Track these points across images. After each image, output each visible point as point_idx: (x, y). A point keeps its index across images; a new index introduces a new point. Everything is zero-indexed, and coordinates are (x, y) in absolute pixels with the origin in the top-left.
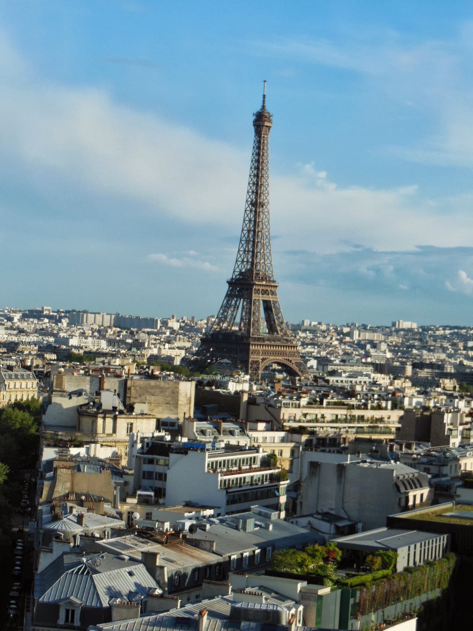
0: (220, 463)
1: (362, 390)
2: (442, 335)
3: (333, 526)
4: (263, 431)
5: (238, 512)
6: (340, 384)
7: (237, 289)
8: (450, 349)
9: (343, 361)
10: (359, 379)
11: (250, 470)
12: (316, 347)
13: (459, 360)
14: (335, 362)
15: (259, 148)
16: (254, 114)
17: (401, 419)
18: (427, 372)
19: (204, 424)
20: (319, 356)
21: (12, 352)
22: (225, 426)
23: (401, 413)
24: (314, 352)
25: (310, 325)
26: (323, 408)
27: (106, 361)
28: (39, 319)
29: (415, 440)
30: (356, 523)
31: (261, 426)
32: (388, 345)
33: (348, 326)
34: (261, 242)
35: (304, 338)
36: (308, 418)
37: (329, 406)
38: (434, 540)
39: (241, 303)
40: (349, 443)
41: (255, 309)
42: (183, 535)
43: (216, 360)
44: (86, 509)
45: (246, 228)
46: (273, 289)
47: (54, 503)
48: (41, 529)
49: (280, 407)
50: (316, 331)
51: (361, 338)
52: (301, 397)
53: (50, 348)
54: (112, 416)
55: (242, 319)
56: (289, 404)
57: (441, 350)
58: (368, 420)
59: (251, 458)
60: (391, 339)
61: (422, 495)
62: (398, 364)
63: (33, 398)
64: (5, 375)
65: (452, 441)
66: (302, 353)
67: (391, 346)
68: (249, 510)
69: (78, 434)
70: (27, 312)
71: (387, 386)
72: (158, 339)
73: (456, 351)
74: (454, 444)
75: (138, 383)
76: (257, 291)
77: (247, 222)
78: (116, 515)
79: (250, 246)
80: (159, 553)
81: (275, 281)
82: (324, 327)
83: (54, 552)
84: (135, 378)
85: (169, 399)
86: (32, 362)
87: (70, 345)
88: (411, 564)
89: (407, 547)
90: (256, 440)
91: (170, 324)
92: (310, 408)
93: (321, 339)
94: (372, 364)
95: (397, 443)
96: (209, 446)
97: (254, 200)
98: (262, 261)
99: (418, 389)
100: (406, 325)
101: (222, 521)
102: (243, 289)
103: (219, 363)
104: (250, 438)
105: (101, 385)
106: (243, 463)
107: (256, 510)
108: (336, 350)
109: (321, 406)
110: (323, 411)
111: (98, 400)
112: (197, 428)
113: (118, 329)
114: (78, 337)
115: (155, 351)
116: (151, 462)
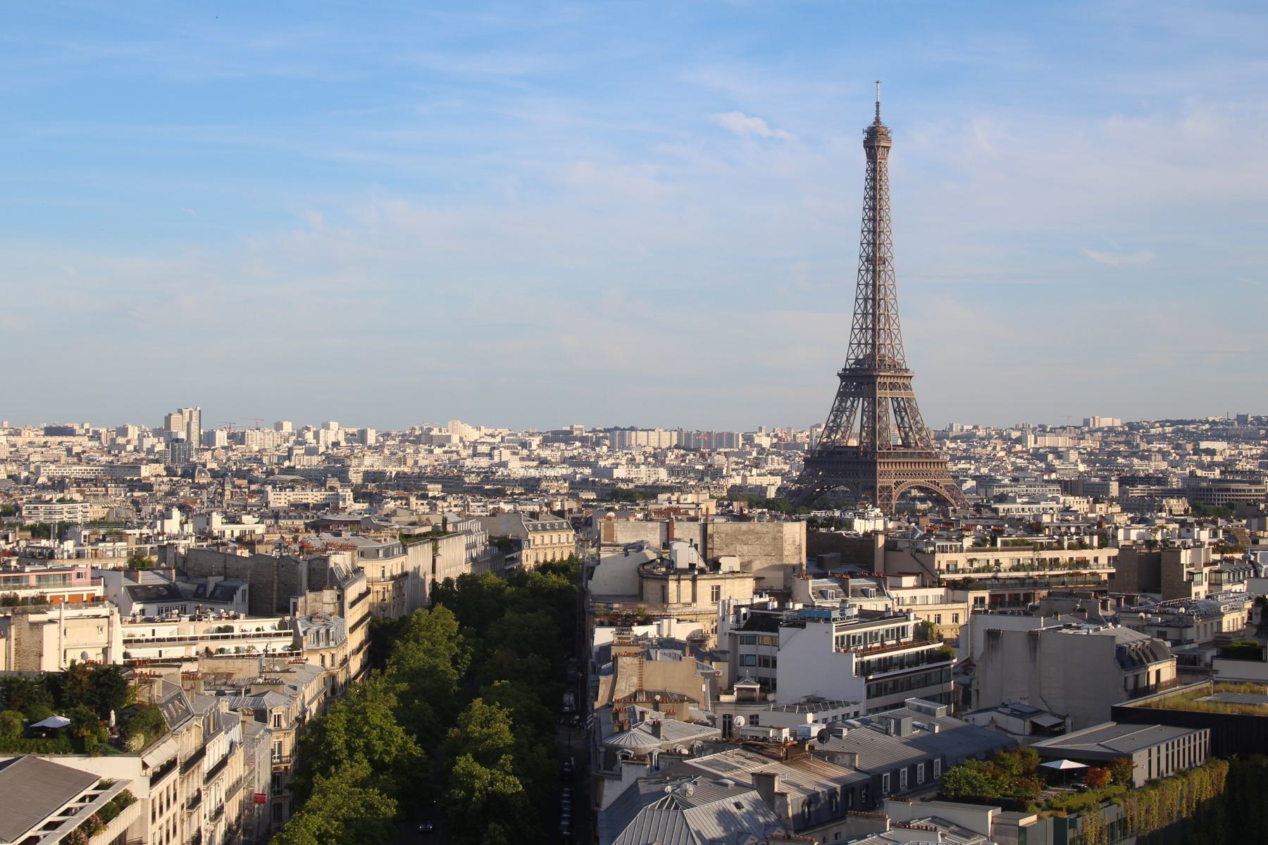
0: (854, 637)
1: (1052, 521)
2: (1159, 434)
3: (1028, 724)
4: (914, 587)
5: (885, 708)
8: (1174, 455)
9: (1015, 480)
10: (1043, 505)
12: (973, 462)
17: (1112, 561)
19: (823, 582)
21: (532, 492)
22: (853, 582)
24: (970, 469)
25: (962, 430)
26: (997, 550)
27: (674, 498)
28: (567, 443)
29: (1139, 592)
31: (908, 581)
32: (1080, 453)
33: (1017, 429)
35: (954, 449)
36: (976, 565)
38: (1187, 738)
39: (860, 404)
42: (809, 746)
43: (829, 487)
45: (861, 296)
46: (905, 381)
47: (616, 706)
49: (934, 552)
51: (1037, 446)
52: (963, 536)
53: (585, 484)
54: (690, 577)
55: (862, 427)
56: (947, 546)
57: (1159, 457)
58: (1065, 566)
59: (898, 629)
60: (1083, 444)
61: (1158, 672)
62: (1097, 480)
63: (571, 555)
64: (527, 526)
65: (1194, 589)
66: (953, 472)
67: (1084, 454)
68: (902, 705)
69: (642, 606)
70: (550, 434)
71: (1086, 513)
72: (740, 463)
74: (1197, 594)
76: (883, 385)
77: (862, 287)
78: (706, 720)
79: (869, 322)
80: (777, 774)
82: (981, 433)
83: (624, 779)
85: (770, 548)
86: (563, 505)
87: (615, 477)
88: (1154, 775)
89: (1146, 752)
90: (899, 600)
91: (757, 441)
92: (977, 551)
93: (979, 450)
95: (1112, 596)
96: (835, 614)
98: (888, 342)
99: (1131, 515)
100: (1106, 422)
101: (865, 723)
102: (862, 383)
103: (833, 492)
104: (893, 599)
105: (666, 533)
106: (887, 635)
107: (913, 704)
109: (995, 548)
110: (997, 555)
111: (667, 555)
112: (813, 588)
113: (682, 452)
114: (626, 466)
115: (737, 480)
116: (752, 641)
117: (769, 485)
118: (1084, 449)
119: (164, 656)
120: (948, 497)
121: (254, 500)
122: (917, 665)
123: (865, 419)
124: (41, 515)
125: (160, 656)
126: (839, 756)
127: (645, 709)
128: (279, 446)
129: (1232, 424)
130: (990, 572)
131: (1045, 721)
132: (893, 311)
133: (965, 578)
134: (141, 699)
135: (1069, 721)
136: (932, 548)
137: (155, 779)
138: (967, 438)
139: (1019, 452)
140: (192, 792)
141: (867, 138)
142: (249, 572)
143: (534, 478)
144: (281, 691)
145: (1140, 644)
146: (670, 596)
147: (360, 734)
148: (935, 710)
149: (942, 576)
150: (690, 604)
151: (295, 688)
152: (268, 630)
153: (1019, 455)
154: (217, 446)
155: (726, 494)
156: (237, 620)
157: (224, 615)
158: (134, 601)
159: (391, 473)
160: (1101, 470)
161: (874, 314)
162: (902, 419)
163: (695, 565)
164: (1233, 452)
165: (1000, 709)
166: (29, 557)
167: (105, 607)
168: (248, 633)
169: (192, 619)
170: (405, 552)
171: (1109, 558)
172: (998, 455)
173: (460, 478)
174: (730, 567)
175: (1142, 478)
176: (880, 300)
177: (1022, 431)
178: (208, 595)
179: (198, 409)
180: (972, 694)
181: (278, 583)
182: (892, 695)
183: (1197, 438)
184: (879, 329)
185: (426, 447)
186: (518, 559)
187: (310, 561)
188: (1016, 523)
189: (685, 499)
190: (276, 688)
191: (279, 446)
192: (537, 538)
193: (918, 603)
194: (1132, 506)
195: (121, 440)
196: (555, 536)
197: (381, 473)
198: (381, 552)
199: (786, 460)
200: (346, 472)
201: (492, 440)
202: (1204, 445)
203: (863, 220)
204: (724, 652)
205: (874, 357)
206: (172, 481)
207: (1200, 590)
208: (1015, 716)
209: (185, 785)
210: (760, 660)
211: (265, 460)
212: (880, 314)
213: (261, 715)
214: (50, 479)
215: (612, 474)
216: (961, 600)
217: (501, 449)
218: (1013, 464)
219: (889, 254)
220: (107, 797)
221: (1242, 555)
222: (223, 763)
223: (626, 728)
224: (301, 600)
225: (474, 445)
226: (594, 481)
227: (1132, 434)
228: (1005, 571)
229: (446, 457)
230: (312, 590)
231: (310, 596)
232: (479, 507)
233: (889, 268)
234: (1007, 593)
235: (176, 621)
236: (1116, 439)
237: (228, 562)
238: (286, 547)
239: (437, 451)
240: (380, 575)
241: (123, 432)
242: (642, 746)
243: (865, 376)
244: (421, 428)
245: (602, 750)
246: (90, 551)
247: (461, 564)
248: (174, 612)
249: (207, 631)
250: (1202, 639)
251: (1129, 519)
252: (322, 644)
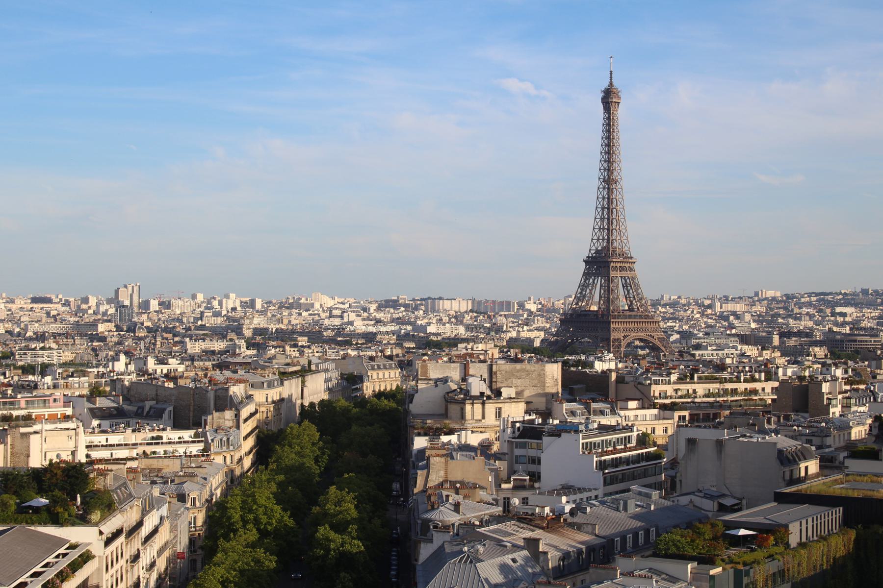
0: (595, 443)
1: (733, 363)
2: (807, 302)
3: (716, 504)
4: (637, 409)
5: (617, 493)
6: (708, 359)
8: (818, 316)
9: (707, 334)
10: (726, 351)
12: (677, 321)
13: (827, 327)
17: (775, 390)
19: (573, 405)
21: (371, 343)
22: (594, 405)
24: (675, 326)
25: (670, 299)
26: (694, 383)
27: (469, 346)
28: (395, 308)
29: (793, 412)
31: (633, 404)
32: (752, 315)
33: (708, 299)
35: (664, 313)
36: (679, 393)
38: (826, 514)
39: (599, 281)
40: (725, 417)
42: (564, 519)
43: (577, 339)
45: (600, 206)
46: (630, 265)
47: (429, 491)
48: (419, 519)
49: (650, 384)
51: (722, 310)
52: (671, 373)
53: (407, 337)
54: (481, 401)
55: (600, 297)
56: (659, 380)
57: (807, 318)
58: (741, 394)
59: (625, 437)
60: (754, 309)
61: (806, 468)
62: (764, 334)
63: (398, 386)
64: (367, 366)
65: (832, 410)
66: (663, 328)
67: (755, 316)
68: (628, 490)
69: (447, 422)
70: (383, 302)
71: (757, 357)
72: (516, 322)
73: (823, 318)
74: (833, 413)
76: (615, 268)
77: (600, 200)
78: (492, 501)
79: (605, 224)
80: (541, 539)
82: (683, 301)
83: (434, 542)
85: (536, 381)
86: (392, 352)
87: (428, 332)
88: (804, 540)
89: (798, 523)
90: (626, 418)
91: (527, 307)
92: (680, 383)
93: (682, 313)
95: (774, 415)
96: (582, 427)
98: (619, 238)
99: (787, 359)
100: (770, 294)
101: (603, 503)
102: (600, 267)
103: (580, 342)
104: (622, 417)
105: (464, 371)
106: (618, 442)
107: (636, 490)
109: (693, 381)
110: (694, 386)
111: (464, 386)
112: (566, 409)
113: (475, 314)
114: (436, 324)
115: (514, 334)
116: (524, 446)
117: (536, 337)
118: (755, 313)
119: (114, 457)
120: (660, 346)
121: (177, 348)
122: (639, 463)
123: (602, 292)
124: (29, 358)
125: (112, 456)
126: (585, 526)
127: (449, 493)
128: (194, 310)
129: (858, 295)
130: (689, 398)
131: (728, 502)
132: (622, 217)
133: (672, 403)
134: (98, 486)
135: (744, 502)
136: (649, 382)
137: (108, 542)
138: (673, 304)
139: (709, 314)
140: (134, 551)
141: (604, 96)
142: (173, 398)
143: (372, 332)
144: (195, 481)
145: (794, 448)
146: (466, 414)
147: (250, 511)
148: (651, 494)
149: (656, 401)
150: (480, 421)
151: (205, 479)
152: (187, 438)
153: (710, 316)
154: (151, 310)
155: (505, 344)
156: (165, 432)
157: (156, 428)
158: (93, 418)
159: (272, 329)
160: (766, 327)
161: (608, 219)
162: (628, 291)
163: (484, 393)
164: (858, 315)
165: (696, 494)
166: (20, 388)
167: (73, 422)
168: (173, 441)
169: (134, 431)
170: (282, 384)
171: (772, 388)
172: (695, 317)
173: (320, 333)
174: (508, 394)
176: (613, 209)
177: (712, 300)
178: (145, 414)
179: (138, 284)
180: (677, 483)
181: (194, 406)
182: (621, 484)
183: (833, 304)
184: (612, 229)
185: (297, 311)
186: (361, 389)
187: (216, 391)
188: (708, 364)
189: (477, 348)
190: (192, 479)
191: (194, 310)
192: (374, 374)
193: (639, 420)
194: (789, 352)
195: (84, 306)
196: (387, 373)
197: (265, 329)
198: (265, 384)
200: (241, 328)
201: (343, 306)
202: (838, 310)
203: (601, 153)
204: (504, 454)
206: (120, 334)
207: (836, 411)
208: (707, 498)
209: (129, 546)
210: (529, 459)
211: (185, 320)
212: (612, 219)
213: (182, 498)
214: (35, 333)
215: (426, 330)
216: (669, 417)
217: (349, 312)
218: (705, 323)
219: (619, 177)
220: (74, 555)
221: (865, 386)
222: (155, 531)
223: (436, 507)
224: (209, 418)
225: (330, 309)
226: (413, 335)
227: (789, 302)
228: (700, 397)
229: (310, 318)
230: (217, 410)
231: (216, 414)
232: (333, 353)
233: (619, 186)
234: (701, 413)
235: (123, 432)
236: (777, 306)
237: (159, 391)
238: (199, 381)
239: (305, 314)
240: (264, 400)
241: (86, 300)
242: (447, 519)
243: (602, 262)
244: (293, 298)
245: (419, 522)
246: (63, 383)
247: (321, 392)
248: (121, 426)
249: (144, 439)
250: (837, 445)
252: (224, 448)
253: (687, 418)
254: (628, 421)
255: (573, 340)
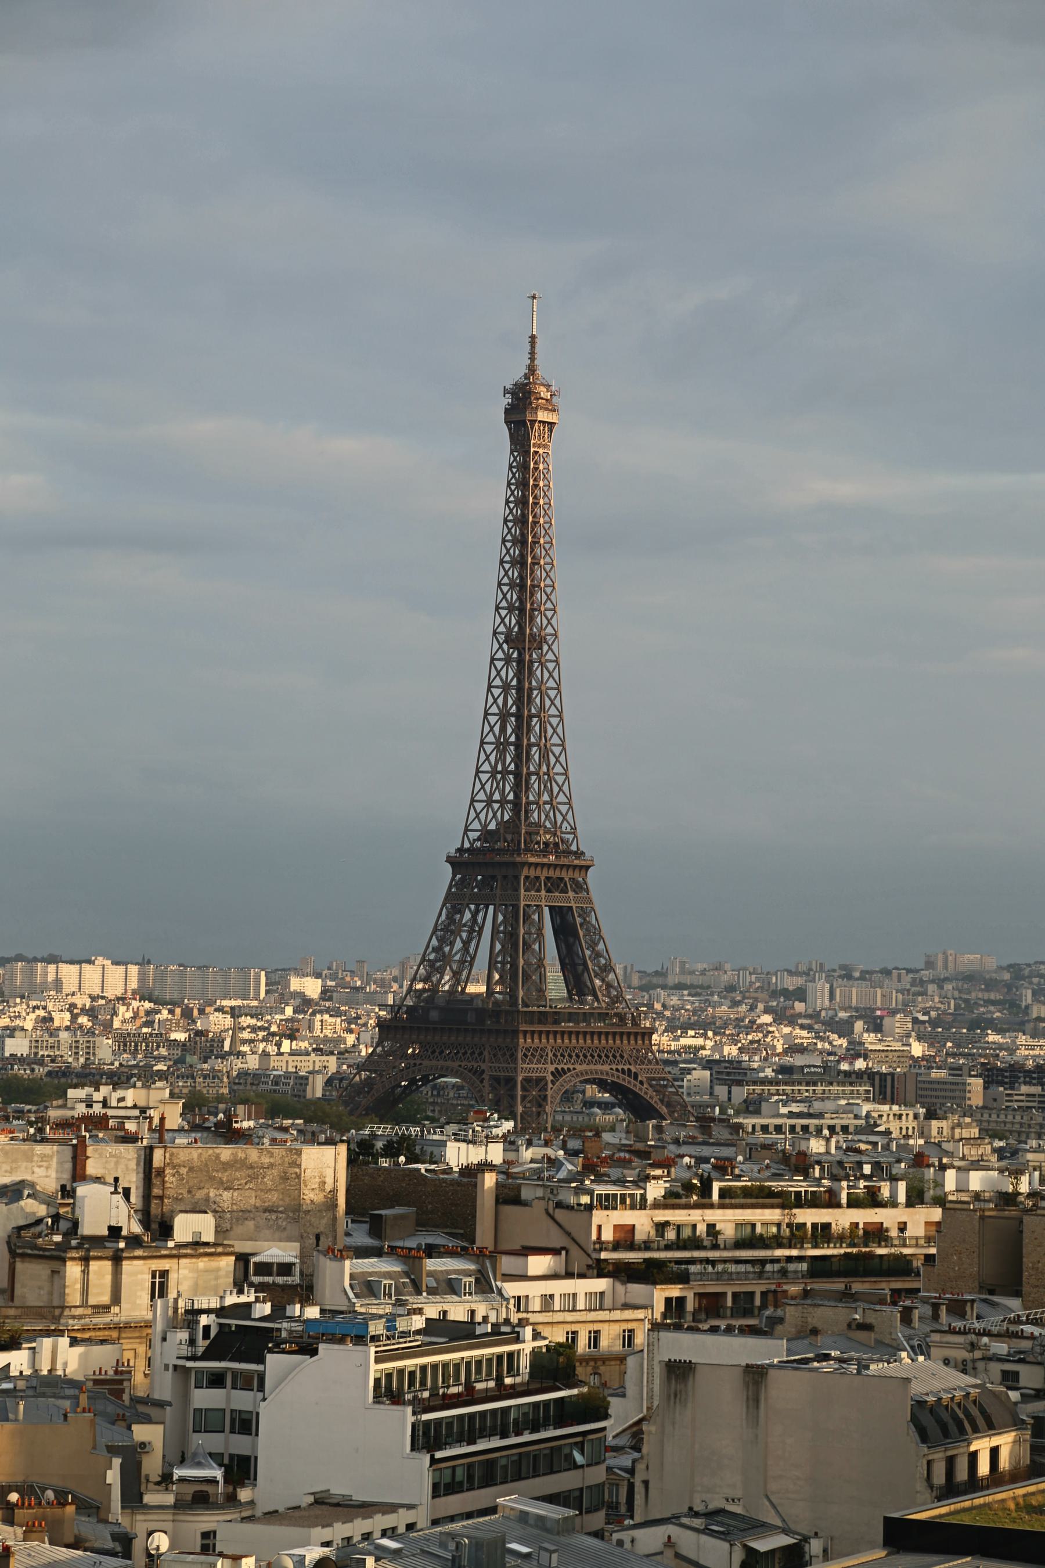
1: (828, 1152)
7: (476, 879)
11: (502, 1392)
12: (710, 1034)
14: (762, 1075)
15: (523, 484)
16: (506, 392)
18: (1028, 1095)
19: (373, 1265)
20: (717, 1057)
23: (936, 1214)
24: (703, 1048)
26: (711, 1206)
30: (806, 1539)
31: (538, 1264)
32: (915, 1021)
34: (538, 745)
36: (671, 1235)
37: (727, 1201)
39: (489, 918)
41: (530, 933)
44: (20, 1531)
45: (494, 710)
50: (709, 987)
52: (647, 1178)
54: (109, 1253)
55: (1026, 996)
59: (500, 1357)
61: (995, 1452)
66: (669, 1052)
67: (924, 1022)
68: (493, 1510)
72: (261, 1028)
75: (183, 1156)
76: (533, 883)
77: (496, 692)
79: (508, 759)
81: (583, 853)
84: (181, 1141)
87: (7, 1054)
92: (674, 1207)
94: (868, 1075)
95: (925, 1301)
97: (516, 629)
98: (546, 797)
100: (969, 960)
102: (493, 878)
105: (78, 1167)
106: (479, 1371)
108: (768, 1040)
109: (706, 1201)
111: (69, 1209)
112: (352, 1277)
113: (148, 1005)
116: (216, 1380)
123: (498, 947)
135: (815, 1547)
138: (701, 987)
145: (959, 1394)
150: (105, 1308)
155: (226, 1091)
160: (954, 1055)
161: (518, 745)
163: (120, 1229)
165: (685, 1520)
172: (759, 1021)
175: (1030, 1071)
189: (122, 1099)
193: (557, 1307)
199: (349, 1023)
204: (161, 1404)
205: (518, 827)
210: (233, 1421)
219: (549, 630)
228: (725, 1248)
243: (501, 864)
251: (994, 1150)
253: (690, 1306)
254: (527, 1312)
255: (413, 1082)
